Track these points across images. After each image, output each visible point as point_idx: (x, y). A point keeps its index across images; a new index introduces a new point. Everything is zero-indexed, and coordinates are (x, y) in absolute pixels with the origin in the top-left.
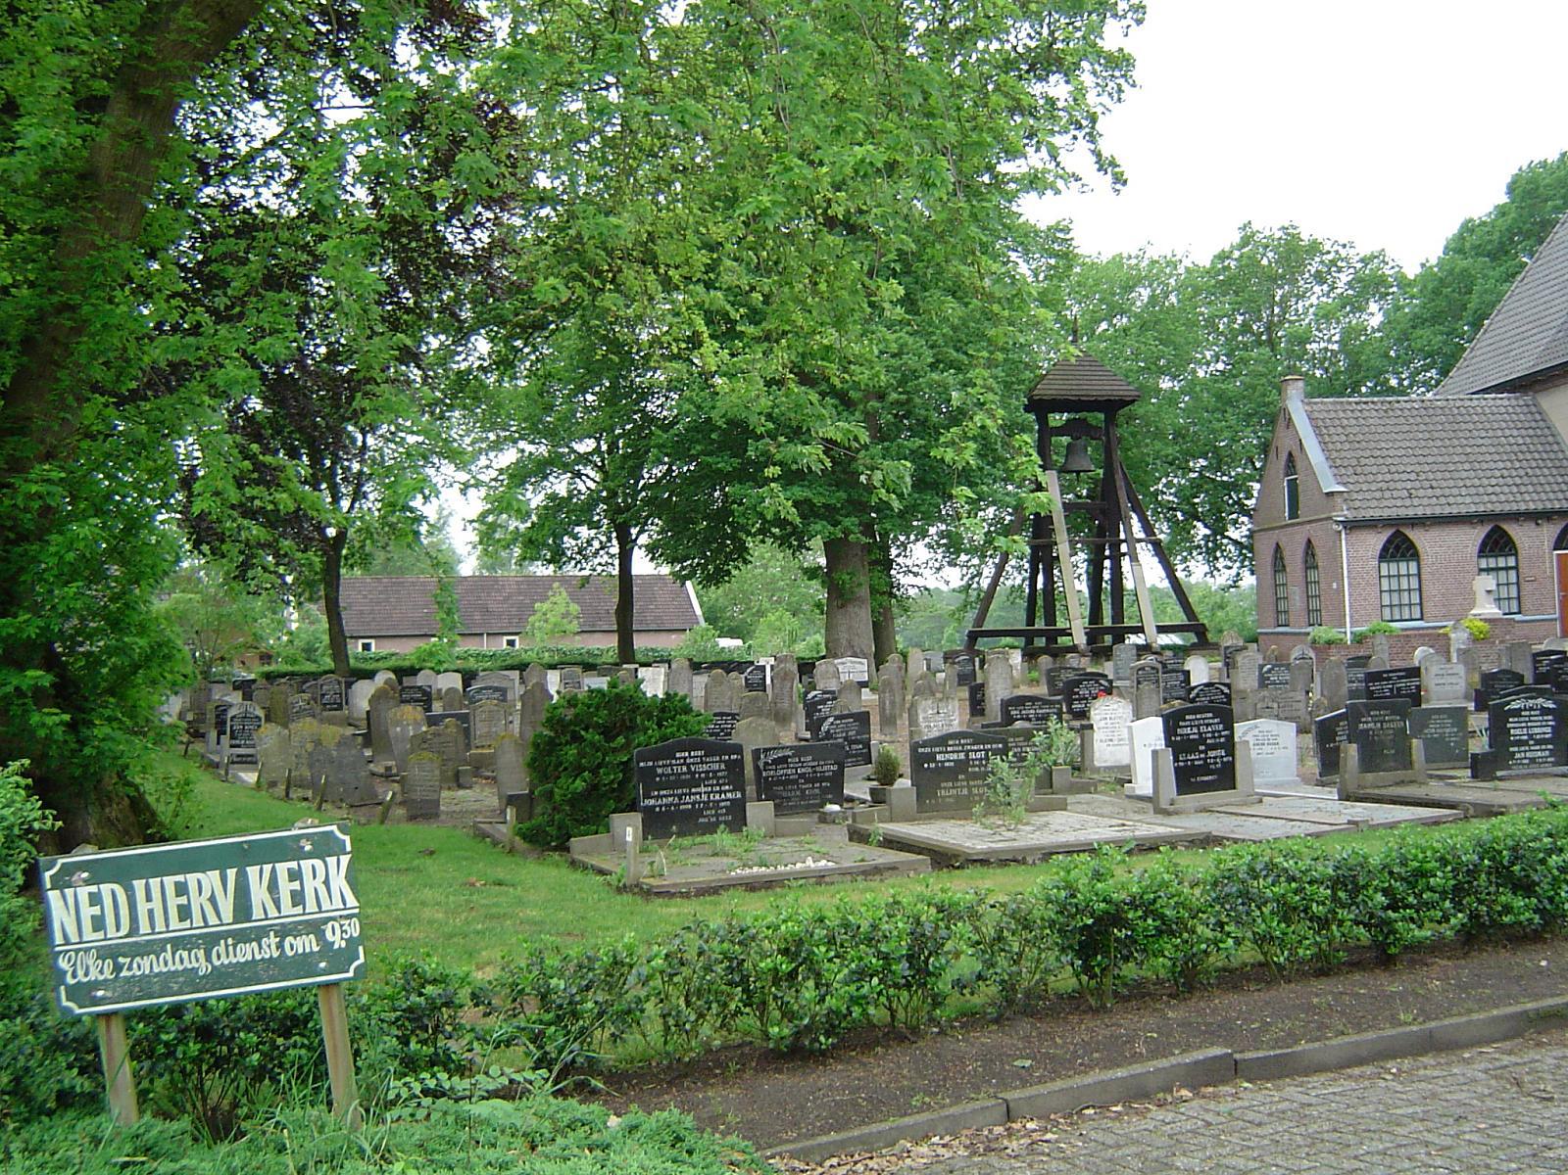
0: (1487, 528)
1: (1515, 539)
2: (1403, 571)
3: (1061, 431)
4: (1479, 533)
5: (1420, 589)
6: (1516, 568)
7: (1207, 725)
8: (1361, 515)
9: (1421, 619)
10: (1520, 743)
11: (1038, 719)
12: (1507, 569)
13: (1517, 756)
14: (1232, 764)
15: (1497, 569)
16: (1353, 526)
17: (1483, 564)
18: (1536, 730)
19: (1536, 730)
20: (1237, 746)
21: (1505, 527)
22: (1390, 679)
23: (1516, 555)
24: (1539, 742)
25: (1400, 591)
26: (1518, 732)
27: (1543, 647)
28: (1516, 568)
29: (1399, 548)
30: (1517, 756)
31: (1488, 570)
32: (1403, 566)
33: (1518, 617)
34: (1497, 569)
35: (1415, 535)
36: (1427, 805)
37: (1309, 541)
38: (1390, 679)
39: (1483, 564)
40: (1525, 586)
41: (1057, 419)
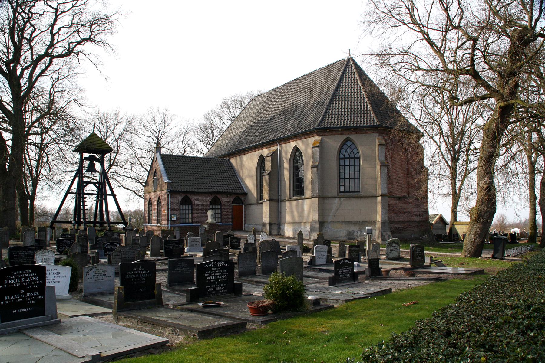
0: (213, 196)
1: (221, 200)
2: (187, 208)
3: (86, 159)
7: (27, 278)
8: (175, 189)
9: (192, 223)
10: (211, 284)
11: (25, 256)
12: (218, 209)
13: (210, 290)
14: (43, 300)
15: (215, 209)
17: (211, 207)
18: (219, 277)
19: (219, 277)
20: (46, 289)
21: (218, 196)
23: (221, 205)
24: (220, 283)
25: (183, 214)
26: (210, 278)
27: (227, 233)
30: (210, 290)
31: (212, 209)
33: (220, 224)
34: (215, 209)
35: (192, 197)
37: (159, 197)
38: (172, 243)
39: (211, 207)
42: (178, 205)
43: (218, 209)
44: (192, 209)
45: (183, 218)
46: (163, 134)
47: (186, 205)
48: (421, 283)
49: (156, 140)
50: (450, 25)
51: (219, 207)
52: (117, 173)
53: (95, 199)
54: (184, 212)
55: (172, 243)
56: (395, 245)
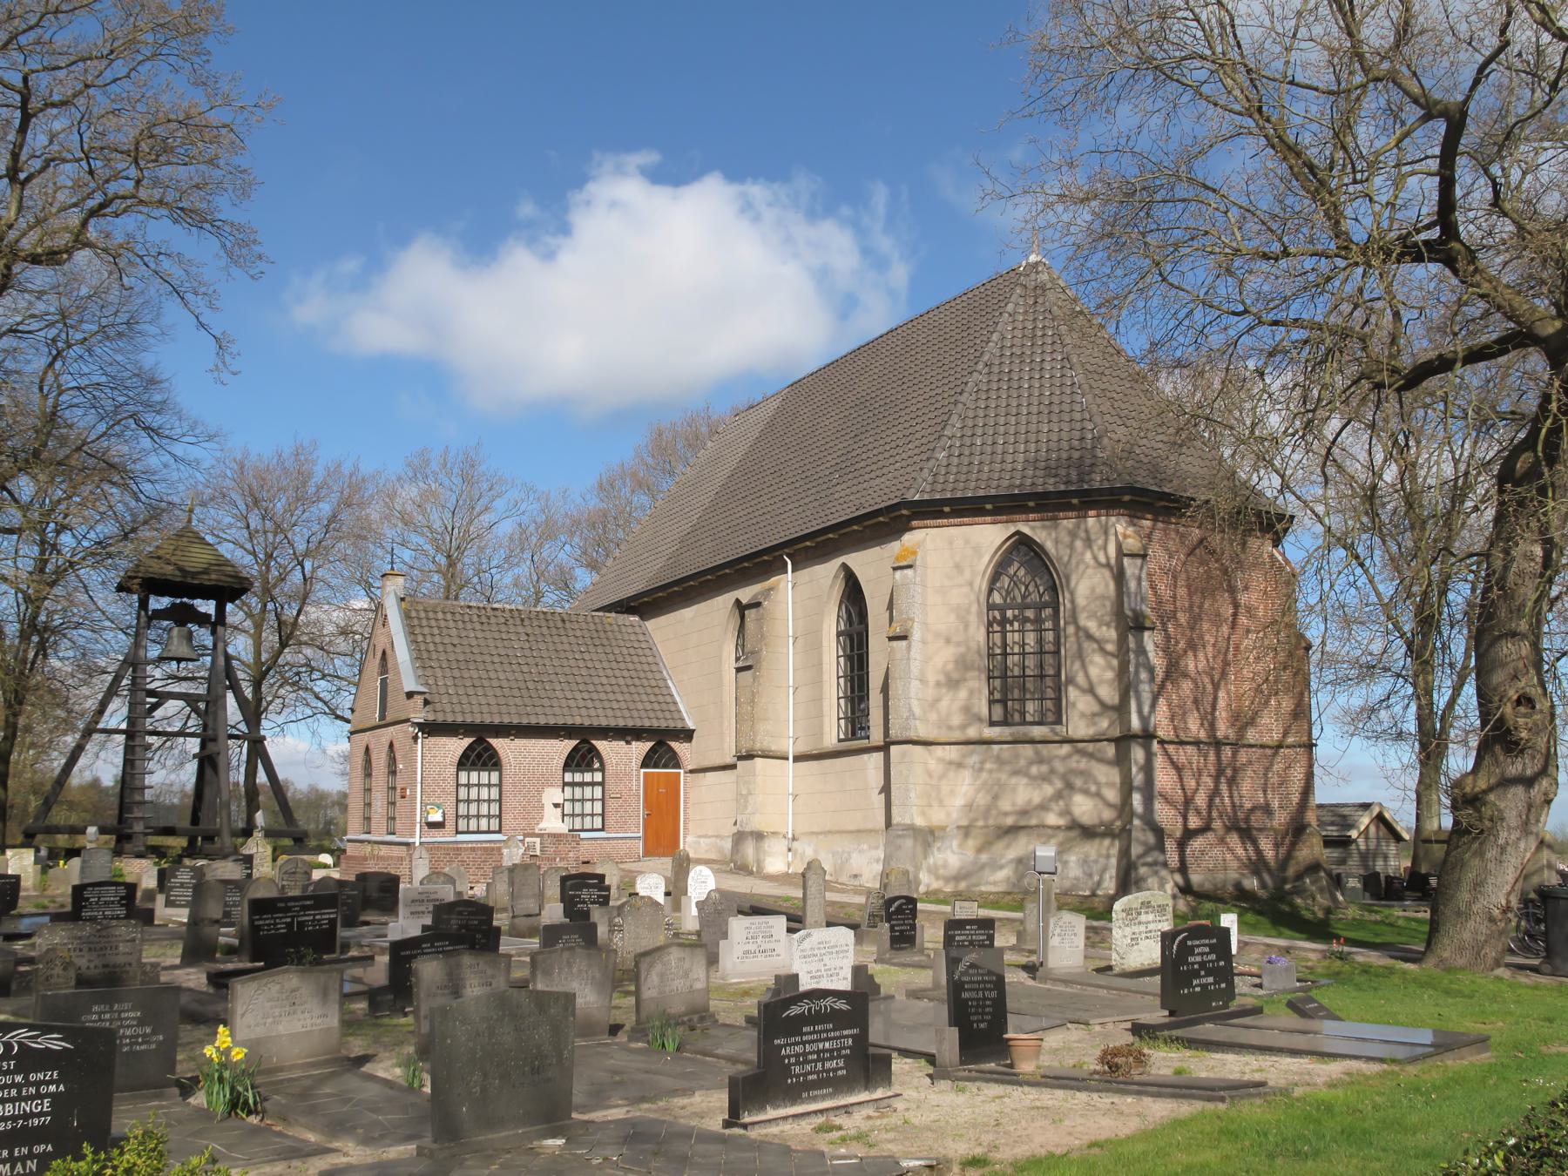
4: (566, 746)
5: (603, 800)
6: (602, 784)
8: (440, 718)
9: (499, 832)
12: (593, 784)
16: (432, 729)
17: (568, 777)
22: (288, 909)
23: (602, 769)
28: (602, 784)
29: (480, 757)
32: (484, 775)
36: (769, 1121)
38: (288, 909)
40: (609, 803)
41: (159, 603)
42: (453, 770)
43: (593, 784)
44: (500, 785)
45: (468, 817)
46: (467, 539)
47: (469, 771)
48: (1160, 1109)
49: (443, 560)
50: (1360, 71)
51: (598, 777)
52: (313, 669)
53: (197, 750)
54: (473, 795)
55: (288, 909)
56: (1151, 917)
